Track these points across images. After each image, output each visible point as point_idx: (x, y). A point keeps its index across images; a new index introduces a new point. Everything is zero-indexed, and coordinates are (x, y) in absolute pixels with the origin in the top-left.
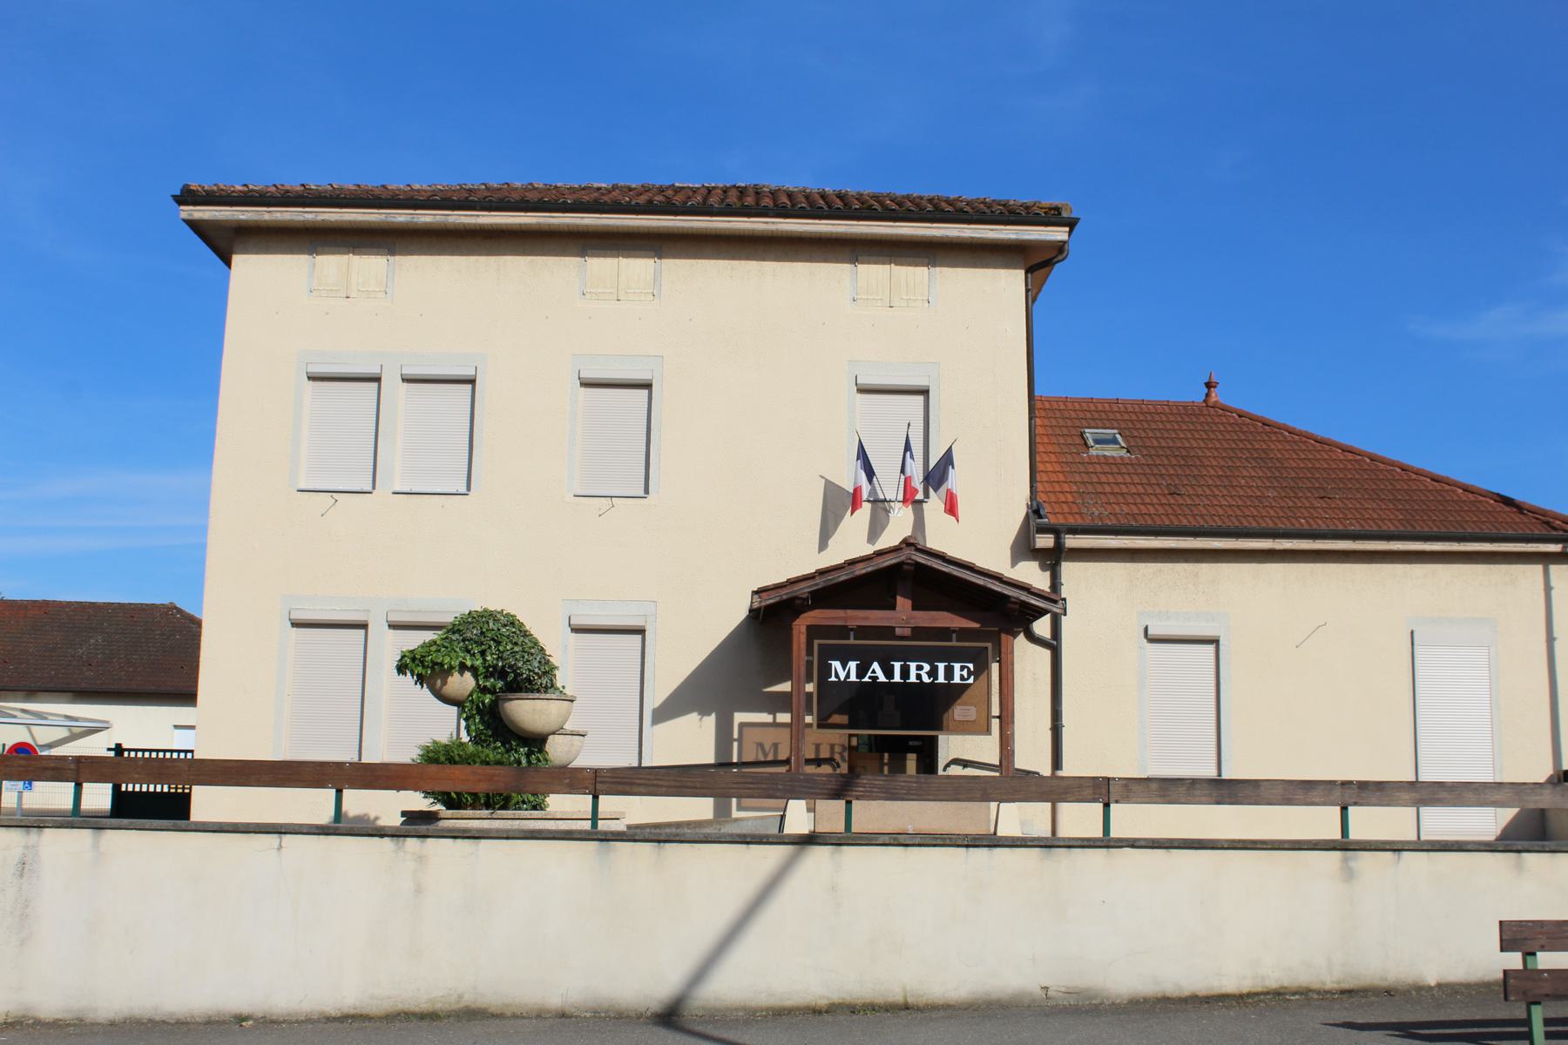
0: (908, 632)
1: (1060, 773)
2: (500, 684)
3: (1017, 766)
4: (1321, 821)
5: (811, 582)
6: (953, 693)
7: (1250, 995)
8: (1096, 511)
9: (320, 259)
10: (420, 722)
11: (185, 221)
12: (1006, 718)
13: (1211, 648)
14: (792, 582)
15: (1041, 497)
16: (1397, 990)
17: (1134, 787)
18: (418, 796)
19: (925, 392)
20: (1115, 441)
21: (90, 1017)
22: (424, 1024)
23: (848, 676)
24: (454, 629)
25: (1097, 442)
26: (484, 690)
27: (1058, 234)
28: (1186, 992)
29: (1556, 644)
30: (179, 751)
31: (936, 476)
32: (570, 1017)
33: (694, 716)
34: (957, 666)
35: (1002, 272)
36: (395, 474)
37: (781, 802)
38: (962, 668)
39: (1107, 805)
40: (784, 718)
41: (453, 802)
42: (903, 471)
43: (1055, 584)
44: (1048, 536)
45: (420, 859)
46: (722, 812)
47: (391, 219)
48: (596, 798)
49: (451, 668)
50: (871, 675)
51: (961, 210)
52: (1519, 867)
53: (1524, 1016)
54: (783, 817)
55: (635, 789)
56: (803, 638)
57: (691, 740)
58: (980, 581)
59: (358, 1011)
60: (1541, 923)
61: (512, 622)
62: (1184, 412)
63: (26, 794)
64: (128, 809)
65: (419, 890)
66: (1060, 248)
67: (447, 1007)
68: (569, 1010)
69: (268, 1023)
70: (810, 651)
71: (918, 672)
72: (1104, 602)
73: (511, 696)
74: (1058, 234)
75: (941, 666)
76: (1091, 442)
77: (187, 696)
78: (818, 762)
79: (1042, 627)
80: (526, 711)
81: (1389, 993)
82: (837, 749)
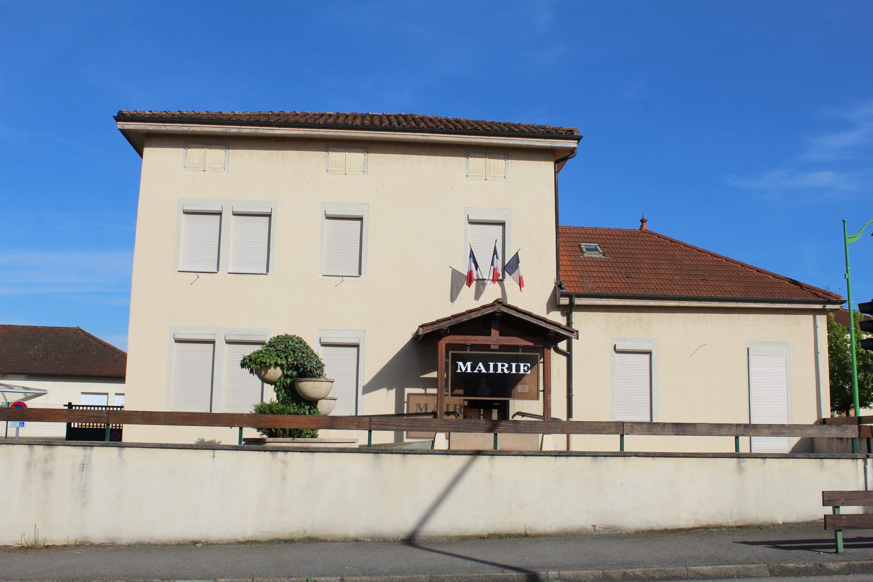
0: (497, 347)
1: (571, 420)
2: (295, 373)
3: (553, 416)
4: (726, 444)
5: (449, 322)
6: (518, 378)
7: (693, 529)
8: (590, 286)
9: (190, 150)
10: (250, 393)
11: (120, 130)
12: (547, 391)
13: (648, 356)
14: (439, 321)
15: (562, 278)
16: (763, 526)
17: (636, 427)
18: (255, 430)
19: (503, 224)
20: (596, 250)
21: (118, 542)
22: (288, 545)
23: (466, 369)
24: (271, 344)
25: (588, 250)
26: (286, 376)
27: (572, 144)
28: (662, 528)
29: (819, 355)
30: (83, 406)
31: (512, 266)
32: (360, 541)
33: (384, 390)
34: (522, 365)
35: (543, 163)
36: (229, 263)
37: (432, 434)
38: (524, 366)
39: (622, 436)
40: (434, 391)
41: (272, 434)
42: (492, 264)
43: (569, 322)
44: (565, 298)
45: (285, 462)
46: (399, 438)
47: (228, 130)
48: (370, 432)
49: (270, 365)
50: (476, 370)
51: (523, 131)
52: (822, 466)
53: (833, 537)
54: (433, 442)
55: (390, 427)
56: (444, 350)
57: (383, 402)
58: (535, 321)
59: (254, 539)
60: (842, 492)
61: (301, 341)
62: (629, 235)
63: (21, 429)
64: (74, 436)
65: (284, 478)
66: (572, 151)
67: (298, 537)
68: (360, 538)
69: (209, 545)
70: (447, 357)
71: (502, 368)
72: (596, 333)
73: (302, 379)
74: (572, 144)
75: (514, 365)
76: (584, 250)
77: (120, 378)
78: (448, 413)
79: (563, 345)
80: (309, 387)
81: (760, 528)
82: (458, 407)
